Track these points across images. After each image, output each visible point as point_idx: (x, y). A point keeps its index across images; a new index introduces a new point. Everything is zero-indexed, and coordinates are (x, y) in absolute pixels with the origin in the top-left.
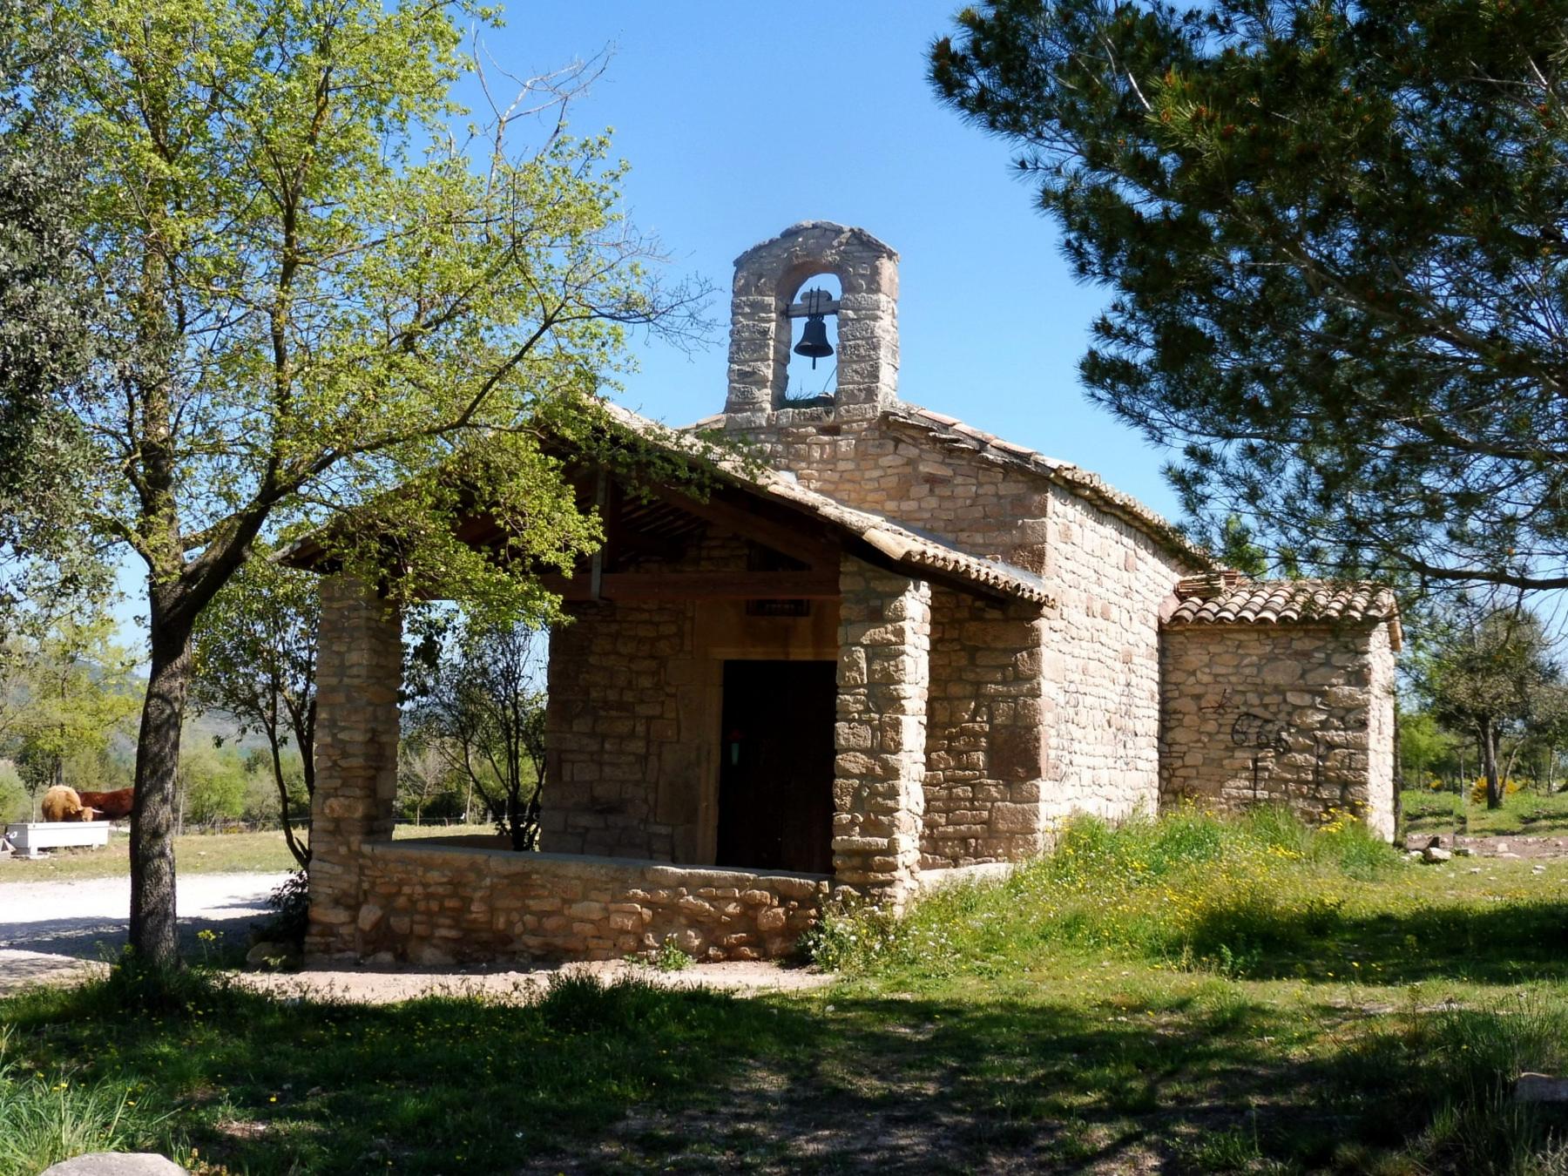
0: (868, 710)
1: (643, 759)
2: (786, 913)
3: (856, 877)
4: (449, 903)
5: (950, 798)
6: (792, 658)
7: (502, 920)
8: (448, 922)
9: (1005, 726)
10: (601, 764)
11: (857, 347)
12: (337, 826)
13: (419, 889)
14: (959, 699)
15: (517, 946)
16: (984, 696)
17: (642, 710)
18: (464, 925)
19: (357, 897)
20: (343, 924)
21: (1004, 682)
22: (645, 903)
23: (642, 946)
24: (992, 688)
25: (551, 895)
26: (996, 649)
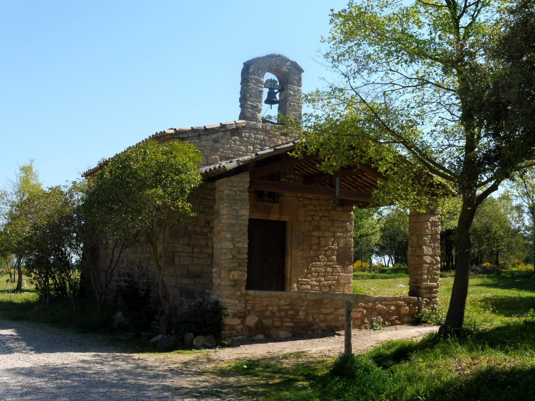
0: (431, 243)
2: (409, 308)
3: (428, 296)
4: (290, 313)
5: (326, 272)
6: (270, 218)
7: (311, 317)
8: (289, 320)
9: (342, 247)
11: (294, 105)
12: (235, 284)
13: (276, 308)
14: (328, 237)
15: (316, 327)
16: (336, 237)
18: (295, 321)
19: (244, 313)
20: (237, 325)
21: (342, 232)
22: (364, 308)
23: (363, 322)
24: (339, 234)
25: (331, 307)
26: (339, 221)
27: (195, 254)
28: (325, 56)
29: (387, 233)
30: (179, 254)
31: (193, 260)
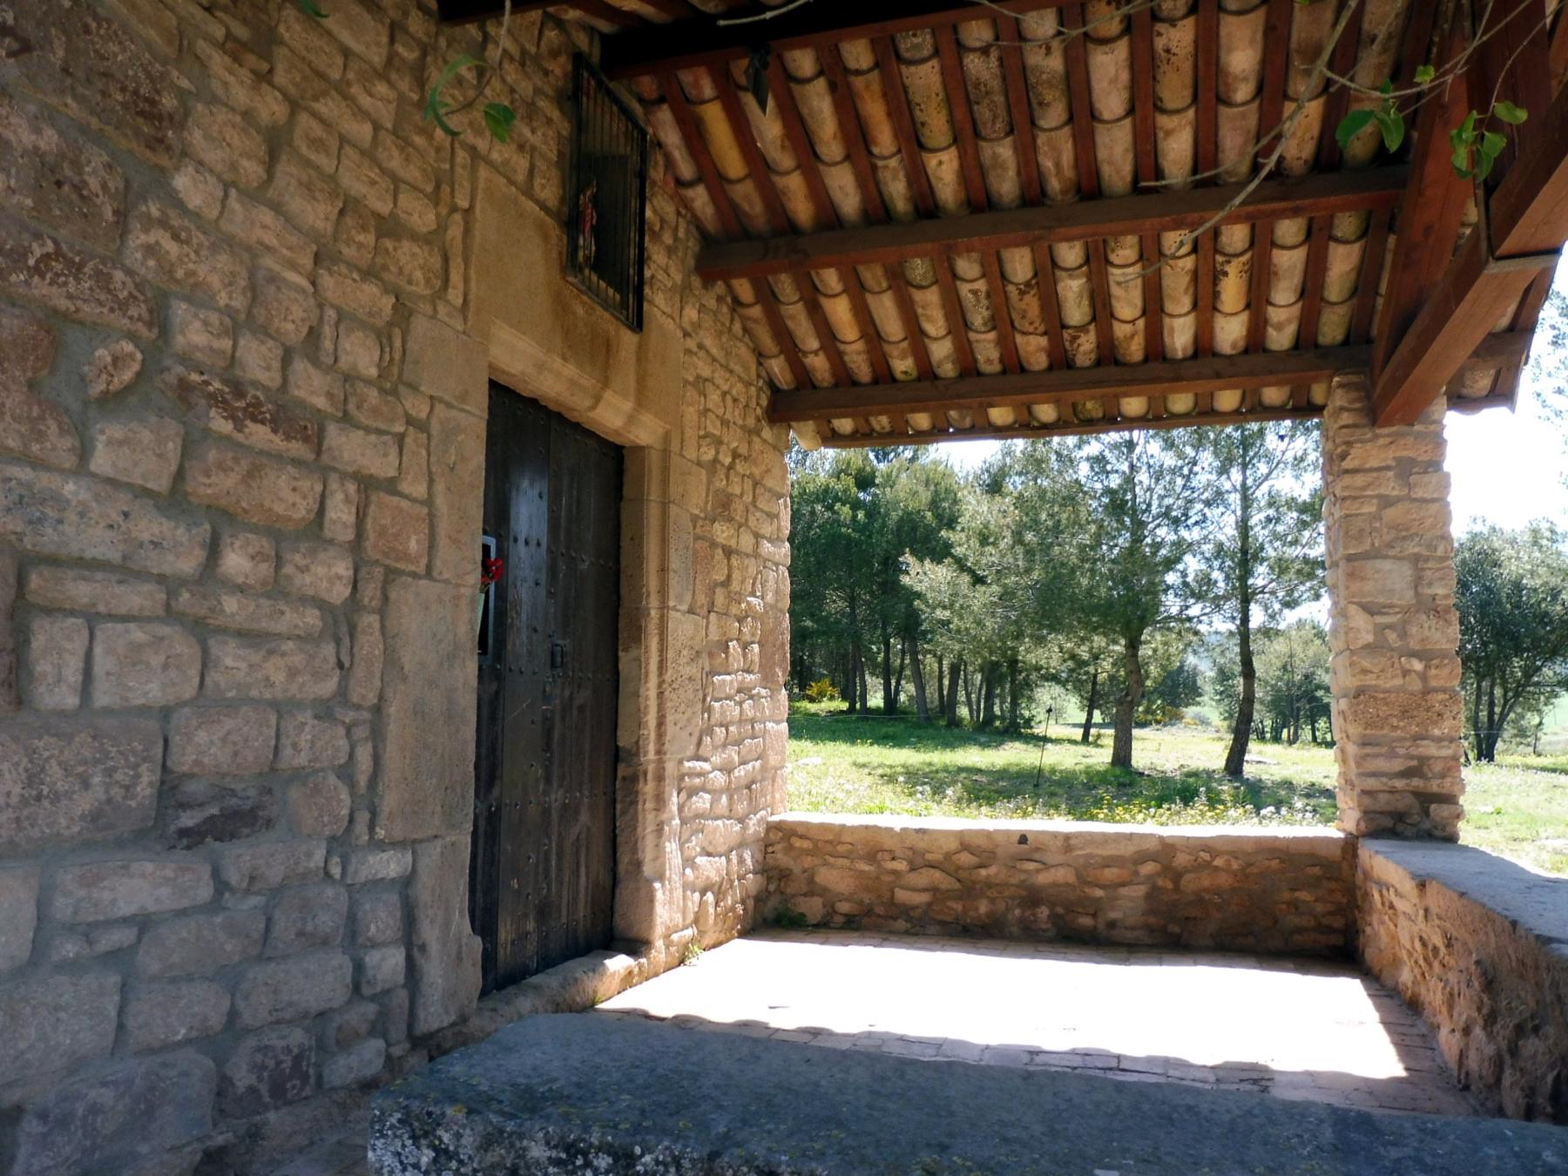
1: (341, 622)
10: (201, 630)
17: (349, 447)
27: (231, 604)
28: (1555, 343)
29: (781, 858)
30: (81, 591)
31: (206, 663)
